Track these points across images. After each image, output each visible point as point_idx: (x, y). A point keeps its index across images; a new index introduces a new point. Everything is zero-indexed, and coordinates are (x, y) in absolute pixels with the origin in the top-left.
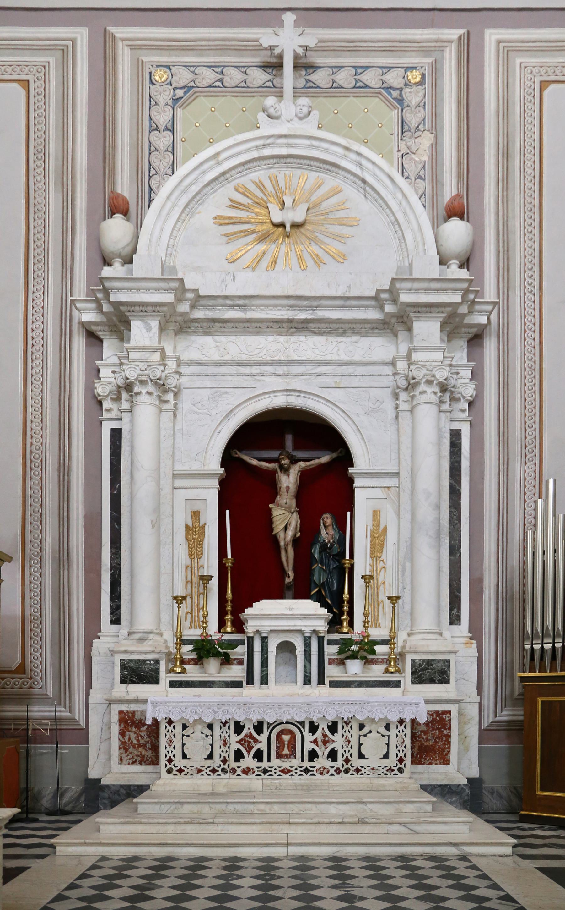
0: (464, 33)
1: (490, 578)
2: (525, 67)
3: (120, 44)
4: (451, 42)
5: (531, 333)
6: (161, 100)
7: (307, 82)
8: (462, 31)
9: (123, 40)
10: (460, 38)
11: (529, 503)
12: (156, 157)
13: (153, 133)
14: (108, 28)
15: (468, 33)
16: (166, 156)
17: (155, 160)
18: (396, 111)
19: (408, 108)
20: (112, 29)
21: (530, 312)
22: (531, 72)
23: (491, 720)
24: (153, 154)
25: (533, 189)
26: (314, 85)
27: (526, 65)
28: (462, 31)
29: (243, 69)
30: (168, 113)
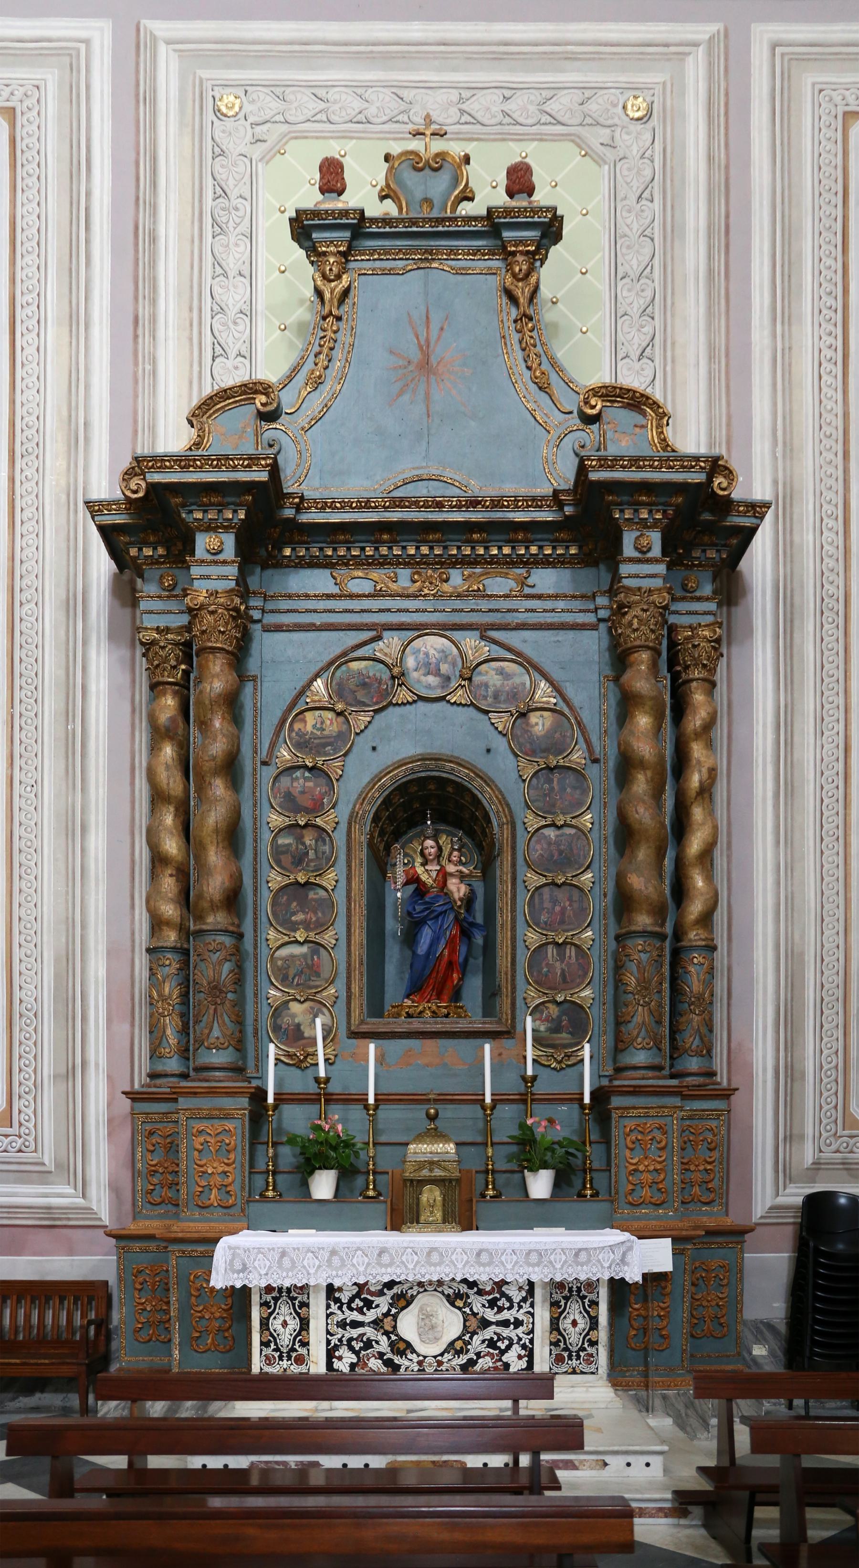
0: (718, 32)
1: (762, 296)
2: (821, 91)
3: (162, 49)
4: (696, 45)
5: (830, 393)
6: (231, 302)
7: (462, 114)
8: (713, 28)
9: (168, 42)
10: (712, 38)
11: (829, 1069)
12: (222, 166)
13: (217, 160)
14: (144, 22)
15: (726, 30)
16: (238, 321)
17: (221, 170)
18: (606, 167)
19: (626, 317)
20: (149, 24)
21: (829, 395)
22: (831, 100)
23: (768, 1204)
24: (217, 360)
25: (833, 268)
26: (472, 120)
27: (824, 86)
28: (713, 28)
29: (359, 89)
30: (241, 249)
